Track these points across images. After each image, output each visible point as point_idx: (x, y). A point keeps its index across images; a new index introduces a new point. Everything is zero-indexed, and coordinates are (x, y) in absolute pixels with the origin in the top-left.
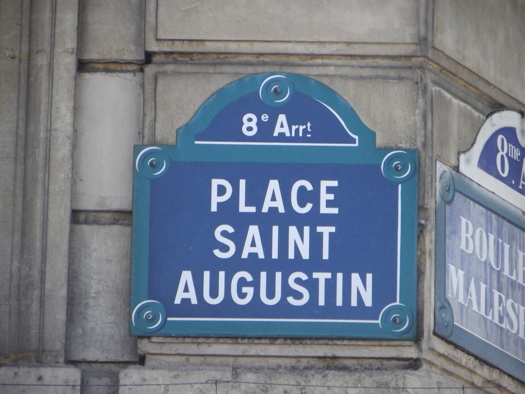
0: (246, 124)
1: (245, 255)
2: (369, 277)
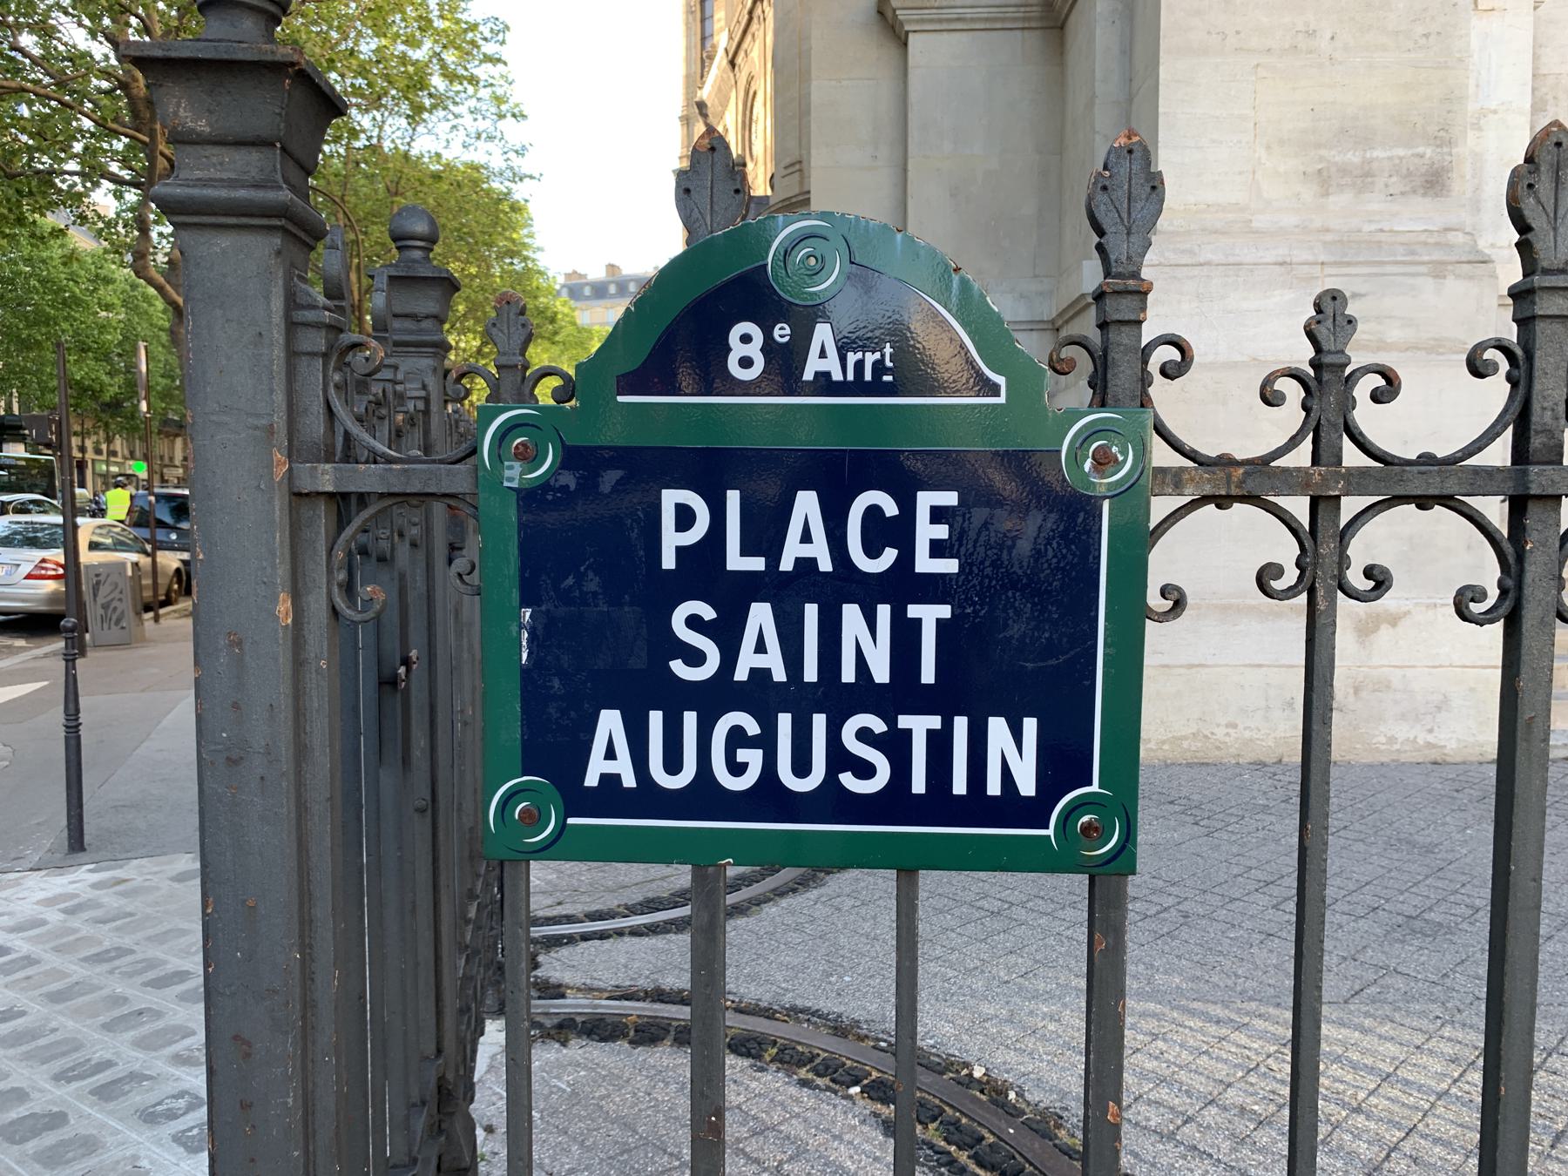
0: (737, 350)
1: (741, 674)
2: (1030, 725)
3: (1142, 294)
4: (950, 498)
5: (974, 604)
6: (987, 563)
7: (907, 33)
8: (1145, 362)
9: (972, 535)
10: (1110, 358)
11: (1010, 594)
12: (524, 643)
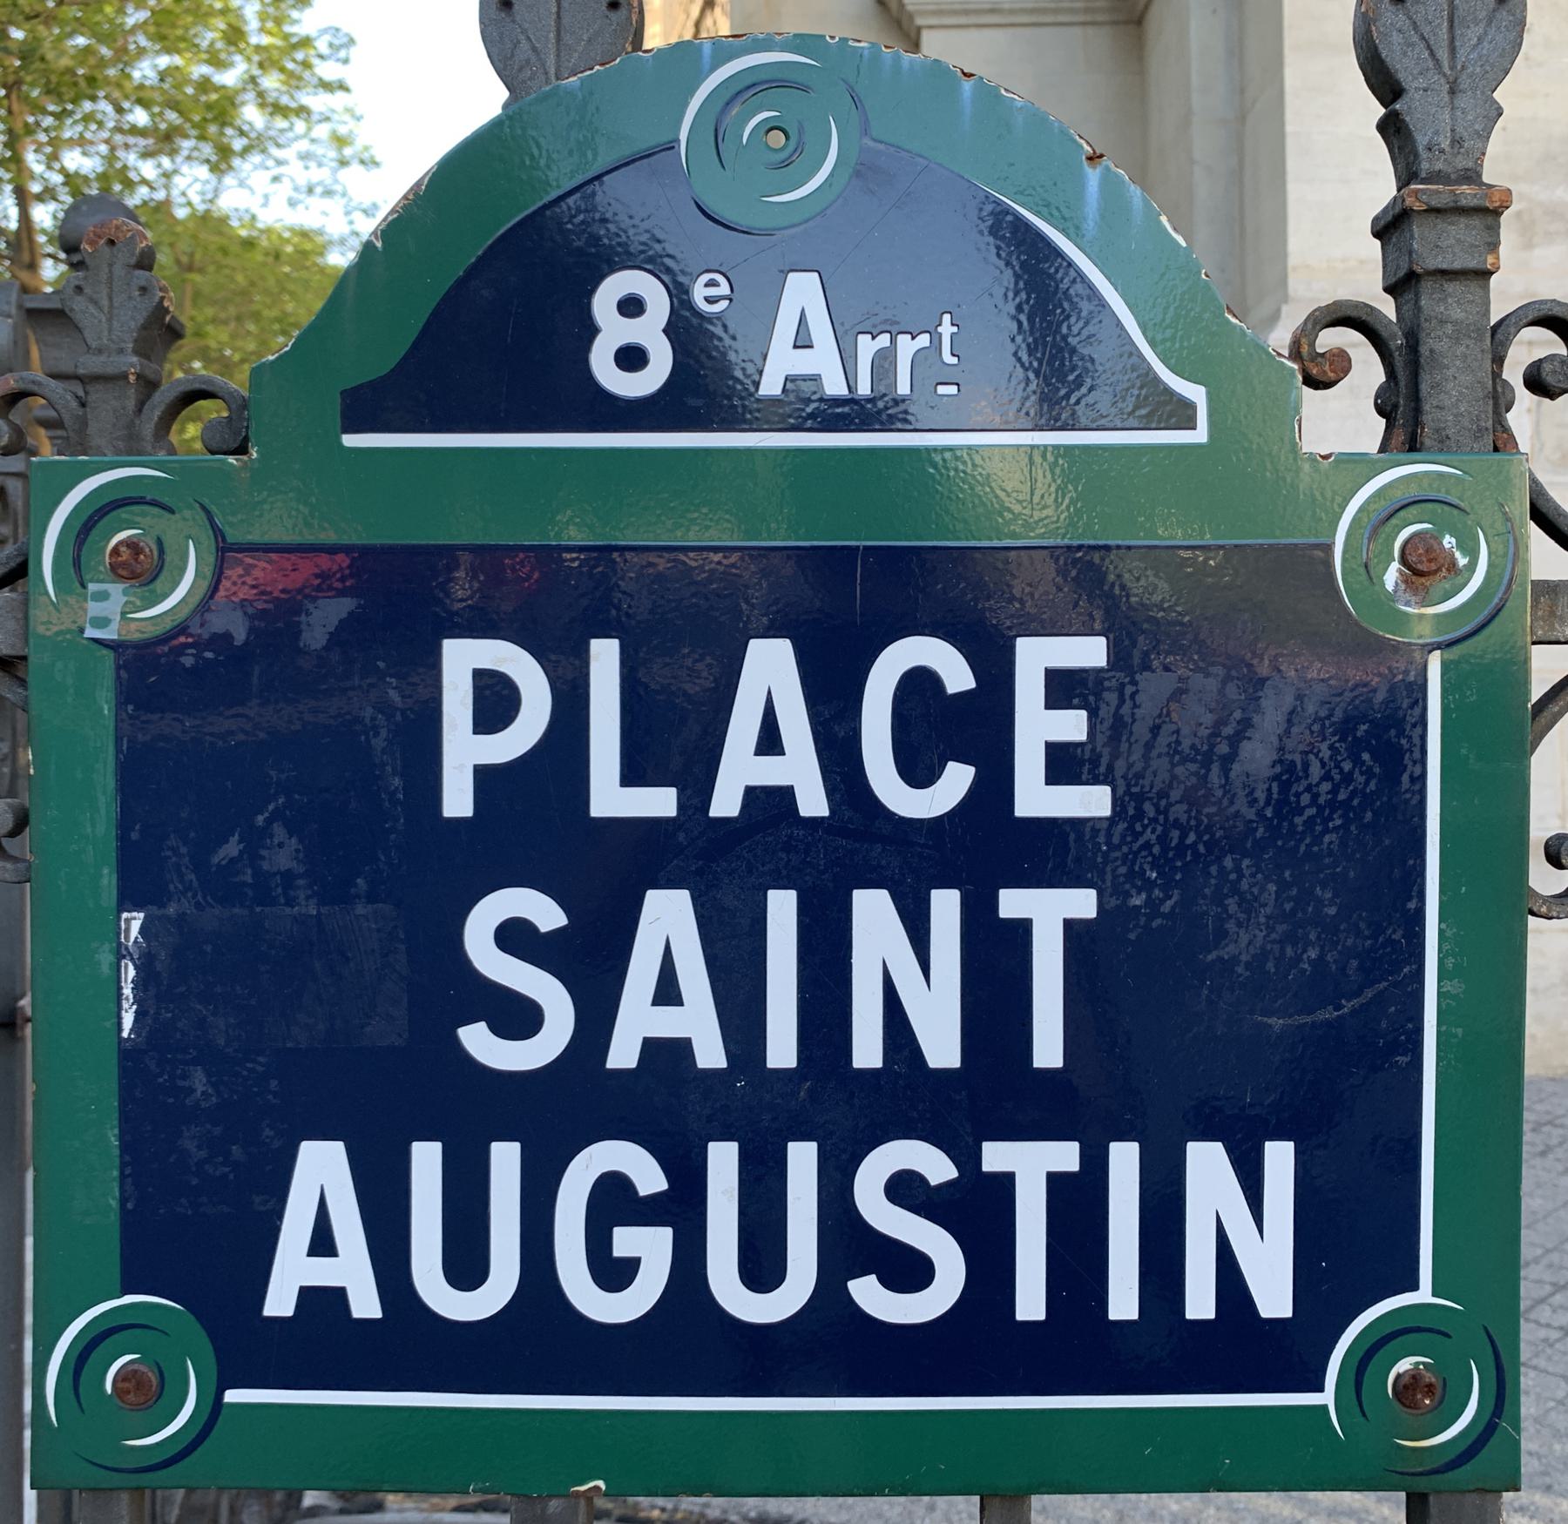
0: (612, 331)
1: (623, 1054)
2: (1279, 1158)
3: (1489, 213)
4: (1089, 652)
5: (1149, 885)
6: (1175, 795)
7: (919, 29)
8: (1499, 360)
9: (1141, 731)
10: (1424, 350)
11: (1228, 862)
12: (127, 991)
